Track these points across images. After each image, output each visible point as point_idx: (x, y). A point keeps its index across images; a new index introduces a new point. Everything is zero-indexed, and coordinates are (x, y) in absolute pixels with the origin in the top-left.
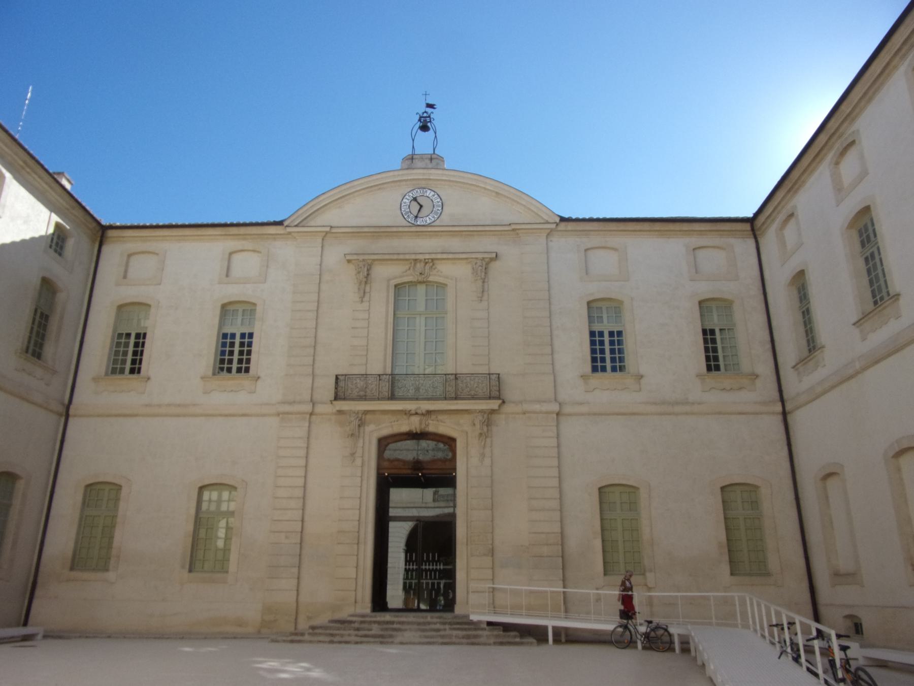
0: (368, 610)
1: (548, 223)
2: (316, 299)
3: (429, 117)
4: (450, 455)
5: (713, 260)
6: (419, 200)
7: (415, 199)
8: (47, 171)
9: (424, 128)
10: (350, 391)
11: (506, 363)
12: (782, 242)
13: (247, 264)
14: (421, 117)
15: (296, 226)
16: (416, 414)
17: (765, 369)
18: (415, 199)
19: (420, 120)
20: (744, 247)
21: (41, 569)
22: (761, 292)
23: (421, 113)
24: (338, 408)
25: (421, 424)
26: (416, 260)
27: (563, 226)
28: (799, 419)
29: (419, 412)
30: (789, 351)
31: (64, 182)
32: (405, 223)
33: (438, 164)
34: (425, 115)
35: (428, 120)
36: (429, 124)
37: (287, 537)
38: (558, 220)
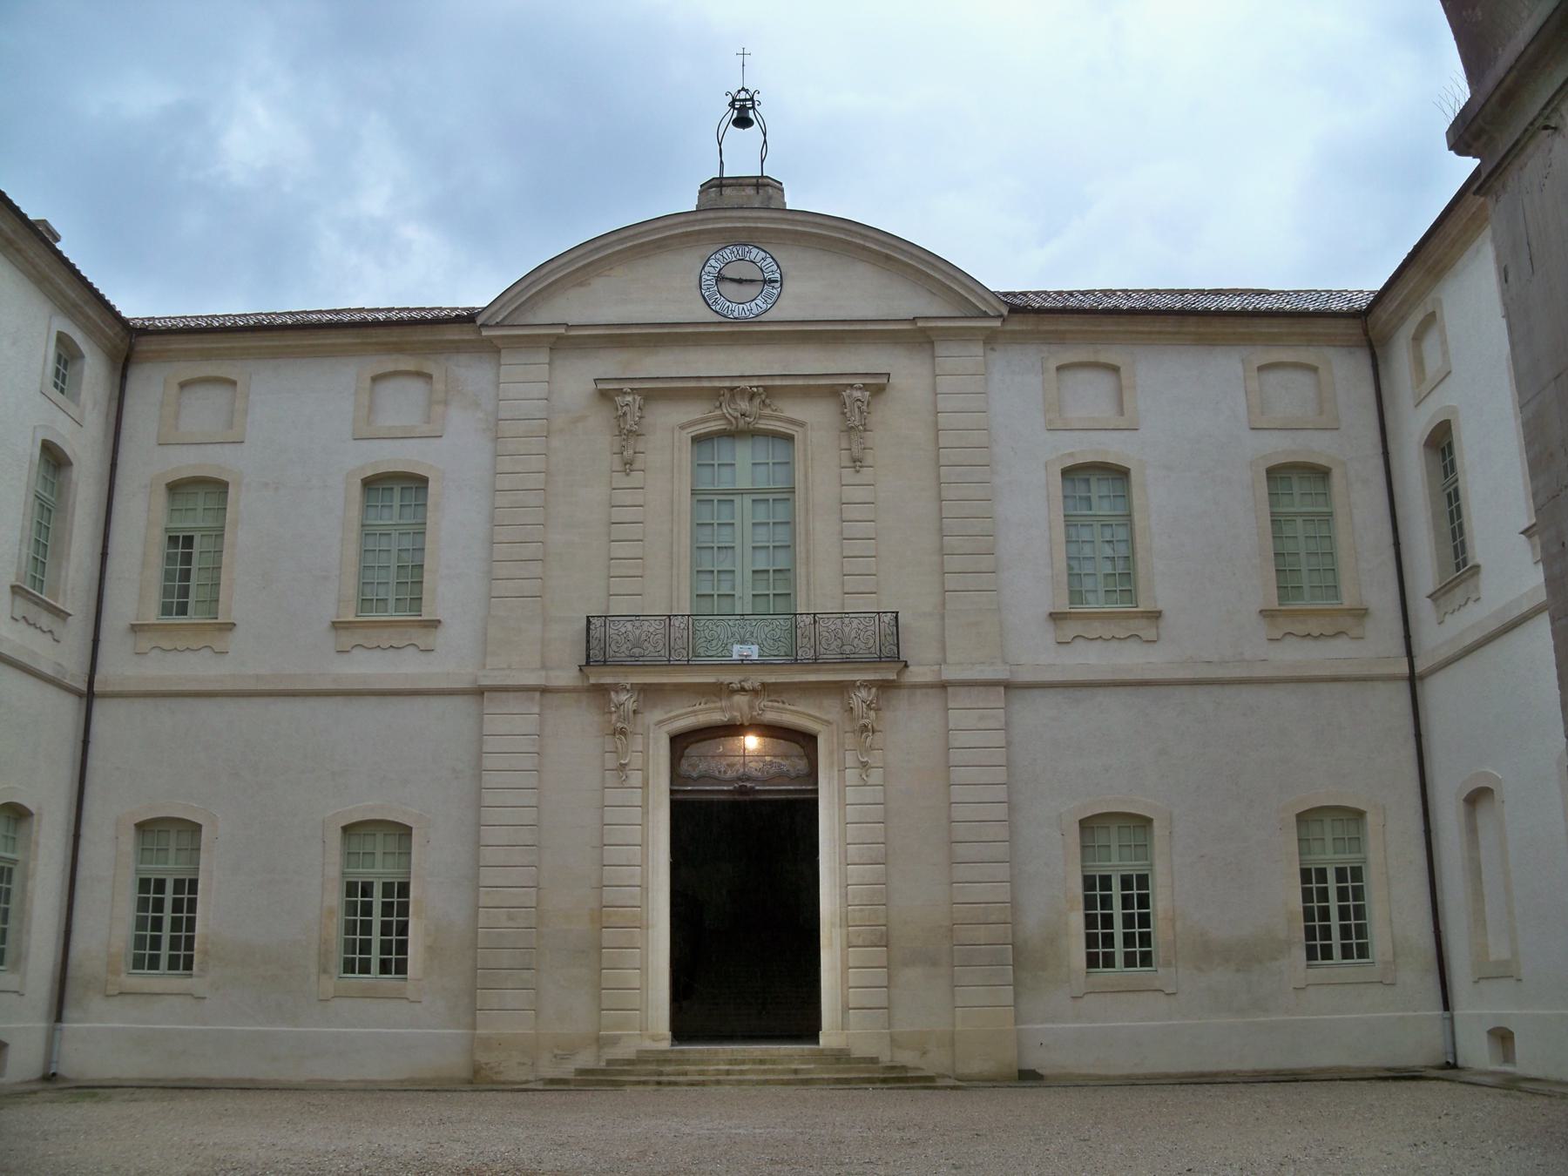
0: (665, 1045)
1: (985, 316)
2: (1405, 670)
3: (752, 99)
4: (802, 765)
5: (1290, 394)
6: (728, 273)
7: (720, 278)
8: (23, 217)
9: (743, 122)
10: (614, 647)
11: (909, 593)
12: (1419, 363)
13: (402, 403)
14: (734, 100)
15: (498, 325)
16: (743, 689)
17: (1383, 600)
18: (720, 278)
19: (732, 105)
20: (1345, 371)
21: (71, 972)
22: (1380, 450)
23: (734, 92)
24: (592, 681)
25: (751, 707)
26: (732, 389)
27: (1016, 325)
28: (1436, 692)
29: (747, 685)
30: (1425, 571)
31: (738, 651)
32: (705, 315)
33: (770, 198)
34: (743, 95)
35: (749, 104)
36: (751, 114)
37: (510, 918)
38: (1005, 311)
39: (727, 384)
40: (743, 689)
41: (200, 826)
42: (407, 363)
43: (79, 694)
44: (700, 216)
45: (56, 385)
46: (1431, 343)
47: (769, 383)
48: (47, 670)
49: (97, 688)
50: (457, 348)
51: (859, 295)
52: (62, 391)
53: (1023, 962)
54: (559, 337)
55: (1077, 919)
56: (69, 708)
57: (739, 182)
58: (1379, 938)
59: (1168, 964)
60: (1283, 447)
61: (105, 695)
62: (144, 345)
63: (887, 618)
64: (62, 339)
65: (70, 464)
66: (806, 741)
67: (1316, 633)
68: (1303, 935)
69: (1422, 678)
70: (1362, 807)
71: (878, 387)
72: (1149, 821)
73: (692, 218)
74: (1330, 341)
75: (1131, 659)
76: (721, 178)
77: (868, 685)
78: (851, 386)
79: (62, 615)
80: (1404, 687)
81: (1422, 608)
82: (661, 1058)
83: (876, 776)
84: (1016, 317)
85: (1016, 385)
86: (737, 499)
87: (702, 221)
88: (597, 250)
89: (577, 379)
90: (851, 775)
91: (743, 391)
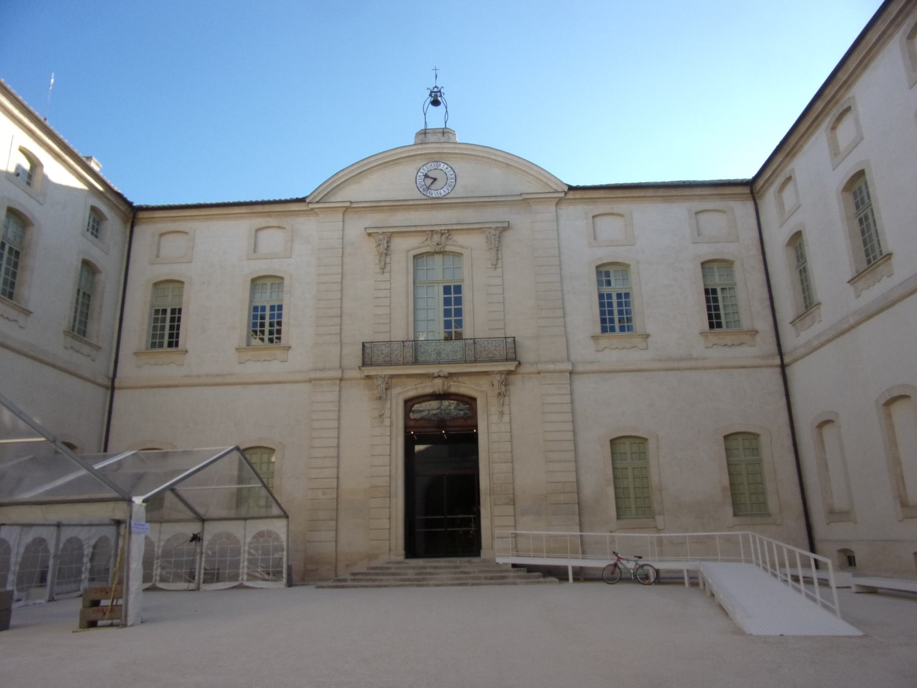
0: (402, 558)
6: (430, 174)
9: (436, 103)
11: (521, 327)
12: (781, 204)
14: (432, 92)
16: (439, 376)
17: (764, 325)
19: (430, 95)
20: (743, 209)
22: (760, 252)
23: (431, 88)
25: (443, 385)
26: (432, 231)
27: (571, 195)
34: (436, 90)
36: (439, 99)
37: (324, 494)
39: (430, 228)
40: (439, 376)
41: (474, 399)
42: (272, 221)
43: (107, 388)
44: (415, 147)
45: (92, 233)
46: (788, 193)
47: (450, 227)
48: (87, 375)
49: (117, 384)
50: (297, 213)
51: (495, 182)
52: (96, 237)
53: (580, 511)
54: (347, 208)
55: (611, 491)
56: (98, 396)
57: (435, 131)
58: (772, 504)
59: (660, 514)
60: (707, 251)
61: (120, 388)
62: (141, 215)
63: (509, 340)
64: (94, 209)
65: (100, 272)
66: (470, 402)
67: (729, 343)
68: (442, 326)
69: (787, 365)
70: (757, 431)
71: (505, 228)
72: (646, 440)
73: (411, 148)
74: (733, 196)
75: (636, 357)
76: (426, 129)
77: (500, 373)
78: (490, 228)
79: (99, 348)
80: (778, 370)
81: (787, 331)
82: (401, 562)
83: (506, 418)
84: (571, 192)
85: (575, 217)
86: (436, 285)
87: (417, 150)
88: (365, 165)
89: (356, 227)
90: (494, 418)
91: (437, 232)
